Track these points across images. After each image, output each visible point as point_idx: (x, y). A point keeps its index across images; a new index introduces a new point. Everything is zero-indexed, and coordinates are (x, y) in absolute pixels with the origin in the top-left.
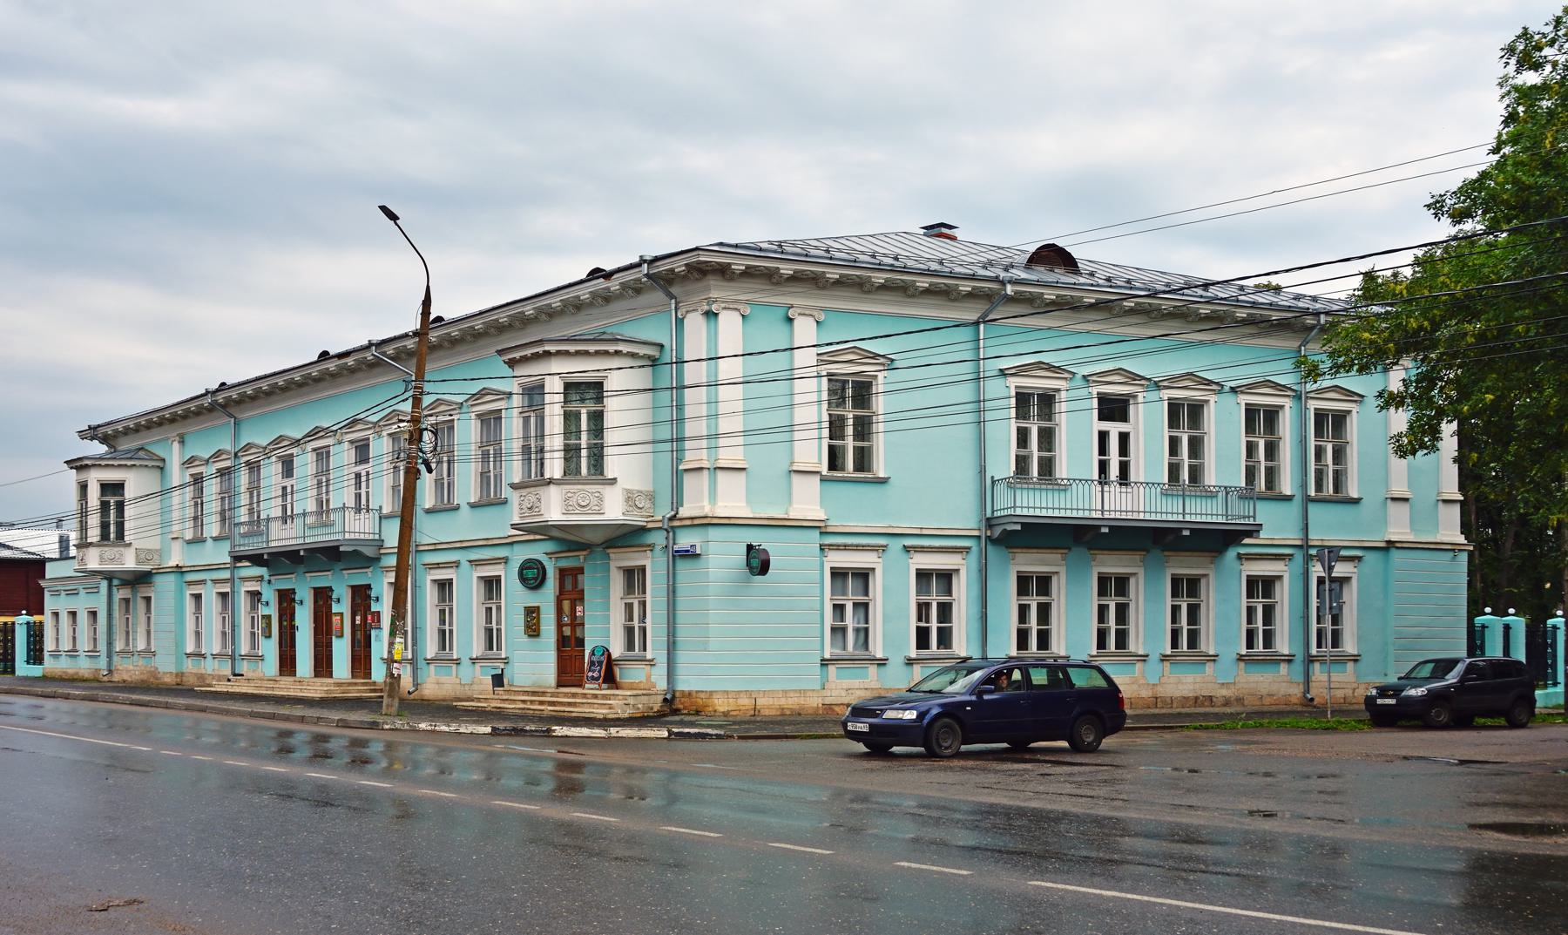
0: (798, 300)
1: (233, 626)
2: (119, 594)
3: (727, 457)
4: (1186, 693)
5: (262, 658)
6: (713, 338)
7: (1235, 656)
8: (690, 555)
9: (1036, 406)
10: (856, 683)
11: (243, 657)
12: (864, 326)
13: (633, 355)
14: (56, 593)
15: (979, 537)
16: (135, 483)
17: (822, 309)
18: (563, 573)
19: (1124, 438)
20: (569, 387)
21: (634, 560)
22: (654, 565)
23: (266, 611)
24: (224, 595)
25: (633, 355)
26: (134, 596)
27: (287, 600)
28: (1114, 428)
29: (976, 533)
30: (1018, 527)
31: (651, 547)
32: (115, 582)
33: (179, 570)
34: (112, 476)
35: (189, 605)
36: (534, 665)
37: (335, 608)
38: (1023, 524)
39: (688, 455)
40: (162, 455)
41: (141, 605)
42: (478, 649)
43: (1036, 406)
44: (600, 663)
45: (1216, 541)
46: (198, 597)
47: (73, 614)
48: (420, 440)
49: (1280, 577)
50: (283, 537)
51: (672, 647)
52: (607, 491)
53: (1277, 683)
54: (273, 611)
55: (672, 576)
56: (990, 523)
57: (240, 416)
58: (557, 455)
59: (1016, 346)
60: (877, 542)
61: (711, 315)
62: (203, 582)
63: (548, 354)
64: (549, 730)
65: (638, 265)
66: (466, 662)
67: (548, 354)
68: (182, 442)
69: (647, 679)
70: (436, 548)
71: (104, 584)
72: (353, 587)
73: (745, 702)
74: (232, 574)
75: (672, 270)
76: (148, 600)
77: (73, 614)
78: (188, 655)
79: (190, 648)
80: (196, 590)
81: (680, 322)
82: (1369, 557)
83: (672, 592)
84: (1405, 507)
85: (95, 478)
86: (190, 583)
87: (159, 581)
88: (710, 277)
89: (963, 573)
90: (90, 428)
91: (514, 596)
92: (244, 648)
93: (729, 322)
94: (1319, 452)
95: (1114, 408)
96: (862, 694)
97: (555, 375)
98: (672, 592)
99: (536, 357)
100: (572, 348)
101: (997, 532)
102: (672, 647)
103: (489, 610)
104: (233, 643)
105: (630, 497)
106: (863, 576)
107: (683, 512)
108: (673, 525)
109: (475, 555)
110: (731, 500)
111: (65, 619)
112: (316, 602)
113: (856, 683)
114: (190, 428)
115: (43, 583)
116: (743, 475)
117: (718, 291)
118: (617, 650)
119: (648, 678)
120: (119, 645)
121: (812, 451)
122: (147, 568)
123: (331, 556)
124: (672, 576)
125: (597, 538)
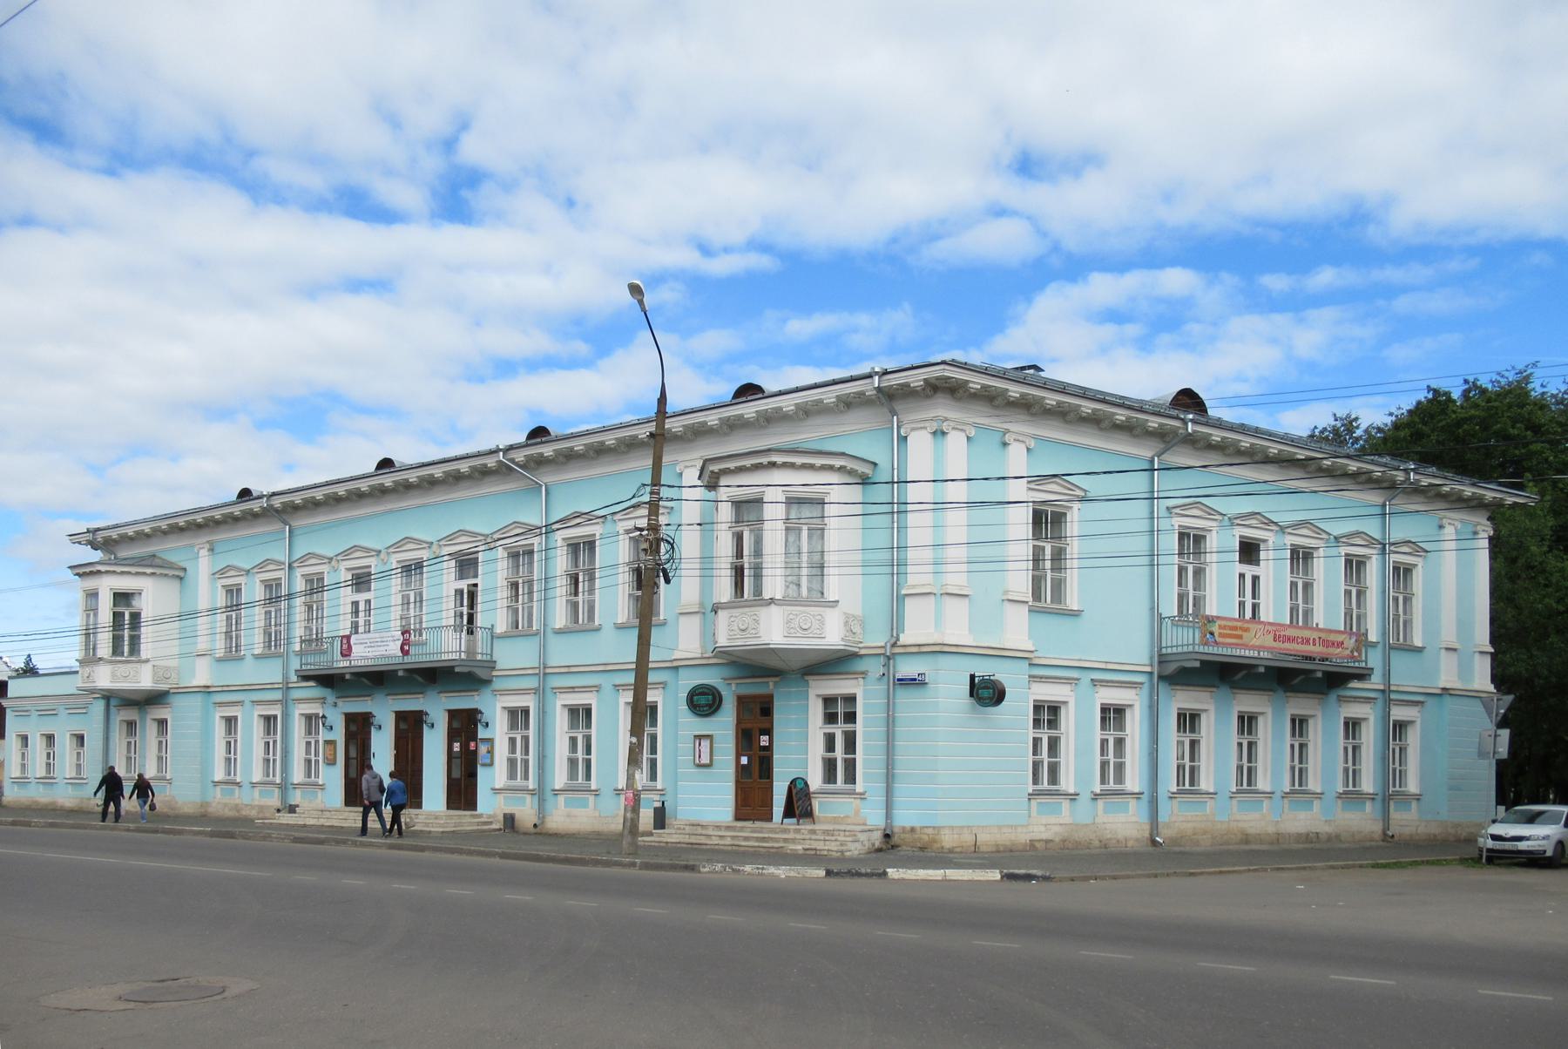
0: (1019, 427)
2: (120, 716)
3: (956, 579)
4: (1302, 830)
5: (322, 787)
6: (939, 460)
7: (1090, 796)
9: (1192, 542)
10: (1053, 819)
11: (296, 786)
12: (1073, 452)
13: (851, 472)
14: (23, 714)
15: (1151, 673)
16: (153, 597)
17: (1034, 437)
18: (742, 701)
19: (1255, 579)
20: (791, 502)
21: (838, 687)
22: (866, 692)
23: (330, 737)
24: (269, 720)
25: (841, 469)
26: (143, 720)
27: (359, 728)
28: (1249, 571)
29: (1148, 669)
30: (1197, 664)
31: (864, 674)
32: (113, 702)
33: (206, 691)
34: (125, 584)
35: (219, 728)
36: (704, 799)
38: (1202, 662)
39: (911, 579)
40: (183, 564)
41: (152, 729)
42: (257, 776)
43: (1192, 542)
46: (230, 722)
47: (50, 738)
48: (658, 552)
51: (890, 778)
53: (1124, 823)
54: (339, 735)
55: (890, 707)
56: (1163, 660)
57: (295, 523)
58: (723, 572)
59: (1188, 479)
60: (1070, 674)
61: (940, 434)
62: (240, 703)
63: (773, 465)
64: (885, 873)
65: (869, 376)
66: (607, 792)
67: (773, 465)
68: (211, 550)
69: (850, 818)
70: (569, 671)
71: (101, 704)
72: (450, 712)
73: (968, 839)
76: (162, 723)
77: (50, 738)
78: (216, 784)
79: (219, 775)
80: (229, 712)
81: (903, 439)
82: (1430, 700)
83: (890, 722)
84: (1453, 657)
85: (106, 586)
86: (221, 704)
87: (177, 701)
88: (939, 394)
90: (88, 531)
91: (675, 723)
92: (298, 775)
93: (956, 440)
94: (1396, 599)
95: (1249, 551)
96: (1057, 829)
97: (775, 487)
98: (890, 722)
99: (757, 467)
100: (799, 460)
101: (1171, 668)
102: (890, 778)
103: (308, 744)
106: (1054, 709)
107: (903, 639)
110: (956, 627)
111: (37, 745)
113: (1053, 819)
114: (220, 536)
115: (5, 703)
117: (942, 409)
118: (815, 781)
119: (857, 812)
121: (1020, 583)
122: (164, 687)
123: (435, 676)
124: (890, 707)
125: (796, 663)
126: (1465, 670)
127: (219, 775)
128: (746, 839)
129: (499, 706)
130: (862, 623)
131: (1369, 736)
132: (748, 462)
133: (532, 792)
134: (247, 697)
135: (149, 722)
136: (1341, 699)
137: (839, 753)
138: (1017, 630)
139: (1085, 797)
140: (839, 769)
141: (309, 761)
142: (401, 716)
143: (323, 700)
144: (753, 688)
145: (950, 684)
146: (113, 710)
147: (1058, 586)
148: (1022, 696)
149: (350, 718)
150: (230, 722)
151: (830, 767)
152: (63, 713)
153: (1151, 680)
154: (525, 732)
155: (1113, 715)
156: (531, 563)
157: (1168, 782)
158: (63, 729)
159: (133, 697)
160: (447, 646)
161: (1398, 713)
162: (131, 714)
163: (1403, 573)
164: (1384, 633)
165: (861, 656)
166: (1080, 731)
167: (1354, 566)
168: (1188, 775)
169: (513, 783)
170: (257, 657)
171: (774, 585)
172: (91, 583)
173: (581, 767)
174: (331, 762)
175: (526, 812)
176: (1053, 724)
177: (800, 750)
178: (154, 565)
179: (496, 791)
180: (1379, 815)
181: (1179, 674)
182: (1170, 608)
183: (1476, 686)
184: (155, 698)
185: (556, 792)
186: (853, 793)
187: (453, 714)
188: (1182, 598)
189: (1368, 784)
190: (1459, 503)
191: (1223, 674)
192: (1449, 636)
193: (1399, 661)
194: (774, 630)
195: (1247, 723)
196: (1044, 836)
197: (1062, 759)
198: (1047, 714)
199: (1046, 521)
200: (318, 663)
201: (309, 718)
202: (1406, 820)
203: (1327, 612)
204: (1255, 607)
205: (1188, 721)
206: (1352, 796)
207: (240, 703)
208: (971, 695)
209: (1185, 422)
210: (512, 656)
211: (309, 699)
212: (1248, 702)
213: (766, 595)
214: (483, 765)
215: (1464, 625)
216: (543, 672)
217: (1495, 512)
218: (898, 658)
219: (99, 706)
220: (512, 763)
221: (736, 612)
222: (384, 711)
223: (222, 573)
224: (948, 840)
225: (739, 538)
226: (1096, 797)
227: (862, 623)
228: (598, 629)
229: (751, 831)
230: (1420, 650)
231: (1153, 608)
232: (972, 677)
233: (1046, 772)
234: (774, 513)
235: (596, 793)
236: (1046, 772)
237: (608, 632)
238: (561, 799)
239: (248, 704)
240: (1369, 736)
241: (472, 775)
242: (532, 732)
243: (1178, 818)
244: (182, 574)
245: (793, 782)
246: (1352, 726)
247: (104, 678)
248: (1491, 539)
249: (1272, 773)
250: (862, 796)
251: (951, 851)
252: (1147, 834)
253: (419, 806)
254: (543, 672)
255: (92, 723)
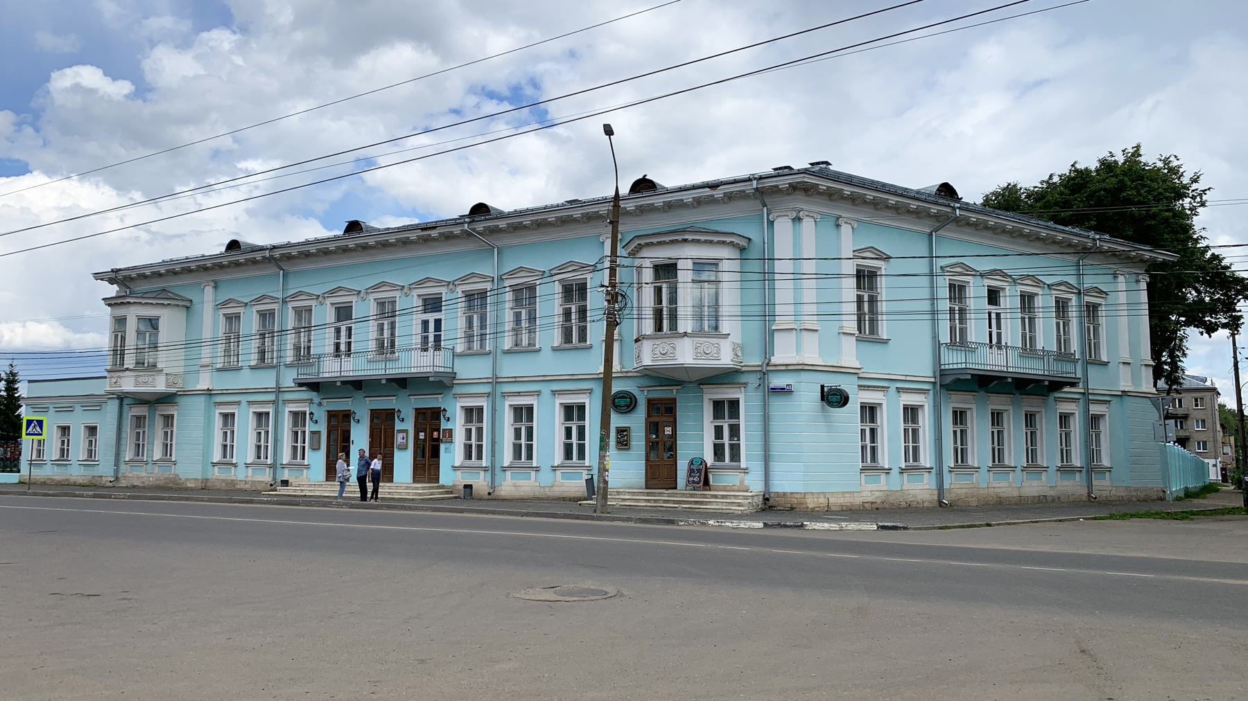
1: (276, 440)
5: (308, 467)
8: (785, 391)
9: (957, 291)
11: (283, 466)
15: (934, 383)
18: (651, 403)
22: (749, 402)
23: (315, 428)
24: (261, 417)
32: (126, 401)
33: (209, 393)
35: (218, 422)
37: (398, 426)
41: (159, 423)
42: (251, 458)
43: (957, 291)
44: (699, 471)
45: (1047, 388)
47: (65, 430)
49: (922, 406)
50: (331, 369)
51: (767, 459)
52: (722, 342)
53: (921, 488)
54: (322, 428)
61: (797, 220)
64: (802, 525)
65: (749, 180)
66: (546, 469)
68: (216, 287)
70: (516, 380)
71: (117, 402)
73: (822, 500)
74: (277, 397)
75: (777, 186)
76: (168, 419)
78: (214, 464)
81: (771, 223)
82: (1114, 400)
83: (766, 419)
85: (132, 314)
87: (183, 401)
89: (926, 407)
90: (112, 271)
93: (808, 225)
96: (878, 494)
97: (686, 256)
98: (766, 419)
101: (949, 380)
102: (767, 459)
104: (493, 455)
105: (735, 347)
107: (774, 360)
108: (765, 372)
109: (556, 387)
110: (811, 354)
112: (372, 421)
114: (221, 276)
116: (816, 334)
117: (800, 202)
118: (709, 458)
119: (742, 482)
120: (128, 455)
121: (851, 325)
122: (173, 390)
126: (1135, 378)
127: (217, 456)
128: (665, 501)
129: (459, 405)
130: (742, 347)
131: (1077, 425)
132: (667, 239)
133: (485, 469)
134: (243, 399)
135: (157, 417)
136: (1056, 399)
137: (726, 439)
138: (849, 354)
139: (895, 472)
140: (727, 451)
141: (225, 446)
142: (375, 414)
143: (311, 401)
144: (660, 393)
145: (807, 392)
146: (126, 408)
147: (873, 322)
148: (858, 397)
149: (331, 415)
150: (228, 418)
151: (718, 451)
152: (78, 408)
153: (934, 387)
154: (479, 425)
155: (911, 413)
156: (484, 305)
157: (949, 461)
158: (78, 422)
159: (146, 398)
160: (415, 361)
161: (1095, 409)
162: (141, 411)
163: (1092, 310)
164: (1083, 353)
165: (743, 372)
166: (890, 424)
167: (1061, 307)
168: (961, 454)
169: (468, 463)
170: (252, 368)
171: (685, 325)
172: (120, 312)
173: (524, 451)
174: (316, 447)
175: (480, 482)
176: (873, 420)
177: (696, 439)
178: (165, 297)
179: (455, 468)
180: (1085, 484)
181: (952, 384)
182: (945, 338)
183: (1144, 390)
184: (166, 399)
185: (504, 469)
186: (739, 468)
187: (420, 412)
188: (952, 329)
189: (1077, 461)
190: (1125, 259)
191: (984, 383)
192: (1125, 355)
193: (1093, 372)
194: (685, 354)
195: (997, 418)
196: (870, 499)
197: (921, 444)
198: (870, 412)
199: (865, 278)
200: (309, 375)
201: (295, 415)
202: (1103, 486)
203: (1045, 338)
204: (999, 335)
205: (959, 417)
206: (1066, 470)
207: (239, 403)
208: (823, 399)
209: (954, 209)
210: (468, 370)
211: (301, 401)
212: (998, 402)
213: (681, 330)
214: (400, 449)
215: (1134, 346)
216: (495, 381)
217: (1152, 266)
218: (771, 375)
219: (113, 406)
220: (468, 448)
221: (658, 342)
222: (362, 409)
223: (225, 304)
224: (811, 503)
225: (658, 291)
226: (902, 471)
227: (742, 348)
228: (539, 350)
229: (663, 497)
230: (1106, 364)
231: (935, 337)
232: (822, 387)
233: (870, 452)
234: (685, 275)
235: (537, 469)
236: (870, 452)
237: (547, 354)
238: (508, 473)
239: (244, 404)
240: (1077, 425)
241: (436, 453)
242: (486, 425)
243: (956, 485)
244: (188, 304)
245: (691, 463)
246: (1064, 419)
247: (128, 384)
248: (1148, 284)
249: (1015, 454)
250: (746, 471)
251: (813, 510)
252: (936, 497)
253: (391, 480)
254: (495, 381)
255: (106, 420)
